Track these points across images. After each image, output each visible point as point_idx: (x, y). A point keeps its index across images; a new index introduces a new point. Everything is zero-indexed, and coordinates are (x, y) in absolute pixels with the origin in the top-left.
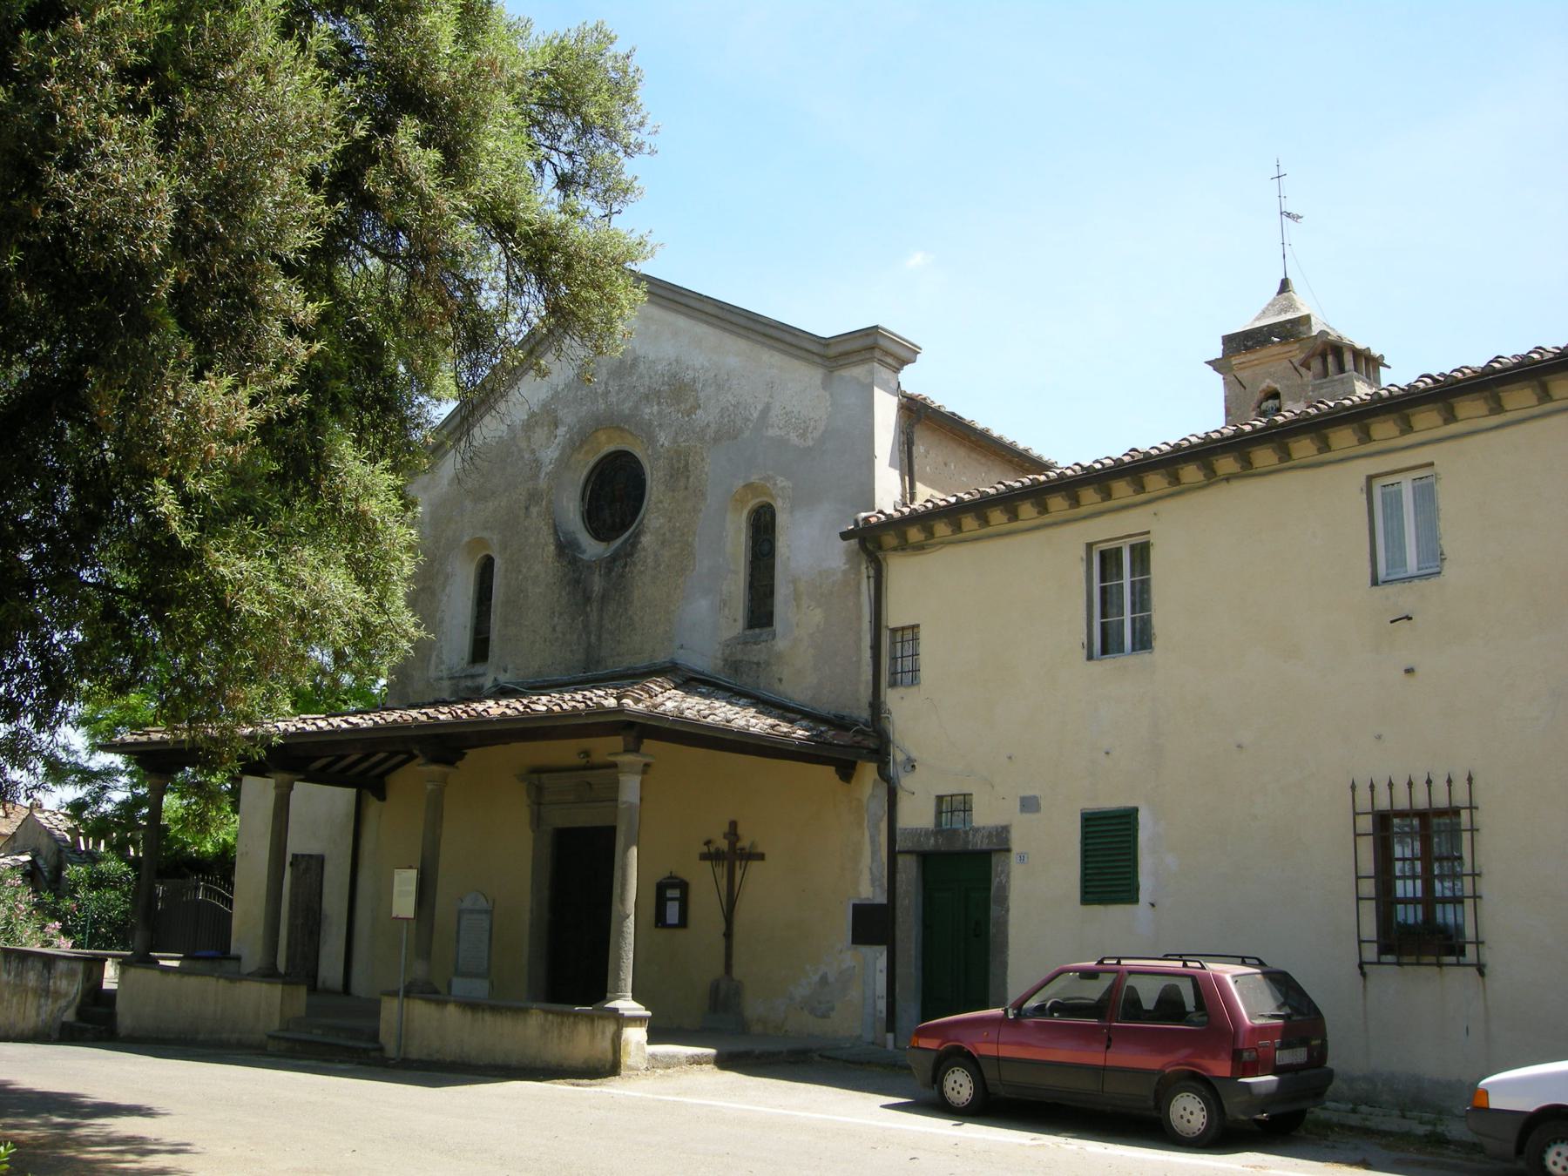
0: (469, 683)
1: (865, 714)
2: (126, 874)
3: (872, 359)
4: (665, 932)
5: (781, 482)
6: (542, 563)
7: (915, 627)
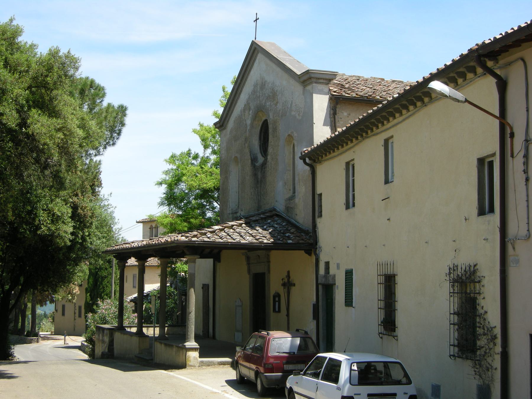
1: (310, 227)
2: (173, 292)
3: (311, 83)
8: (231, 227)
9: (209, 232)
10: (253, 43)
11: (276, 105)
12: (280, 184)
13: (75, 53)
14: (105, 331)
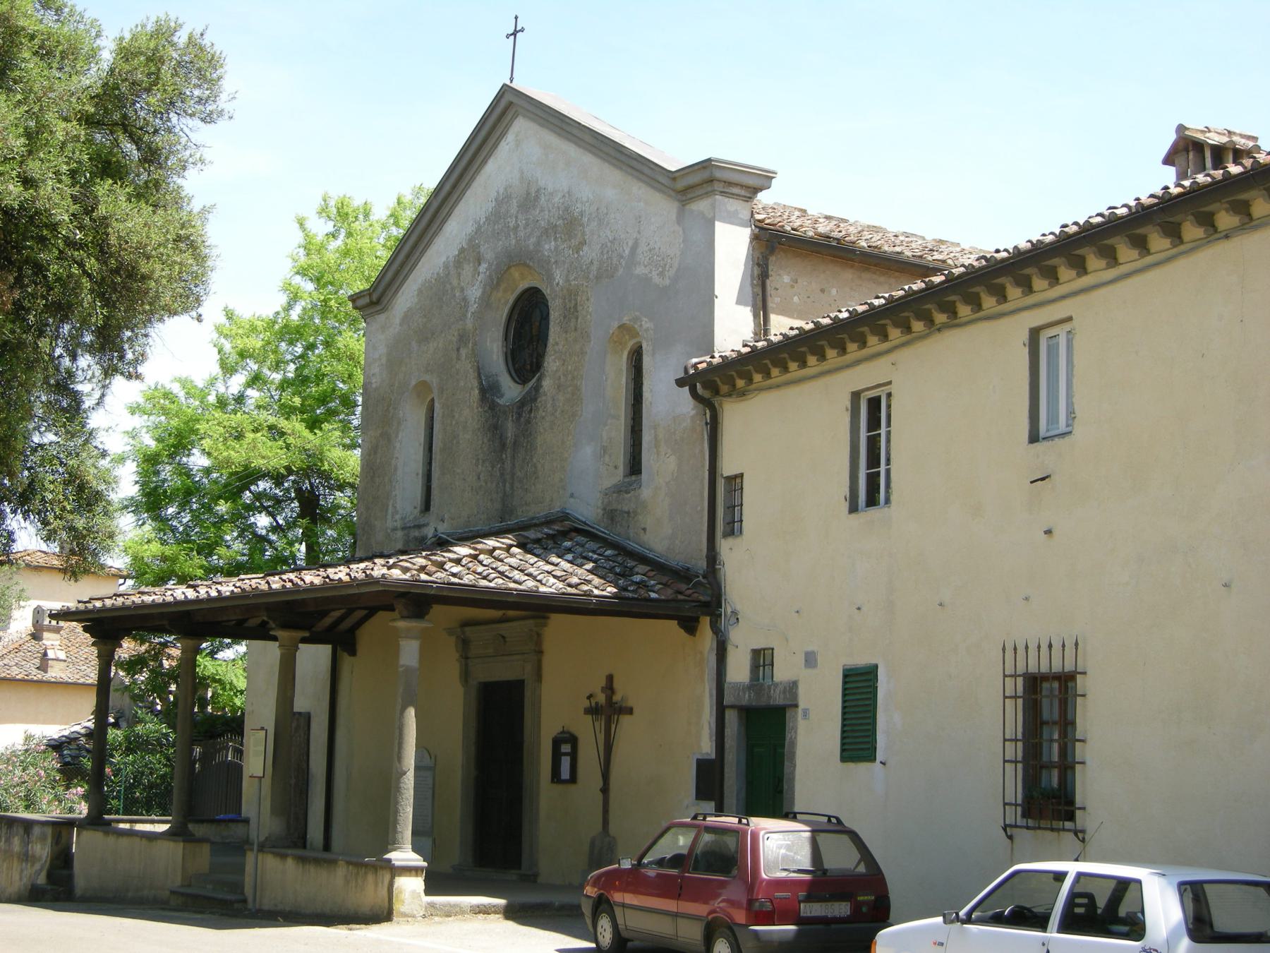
0: (416, 533)
1: (702, 564)
2: (166, 735)
3: (713, 192)
4: (560, 787)
5: (646, 324)
6: (469, 413)
7: (742, 475)
8: (491, 552)
9: (451, 560)
10: (505, 90)
11: (578, 249)
12: (587, 452)
13: (216, 41)
14: (37, 830)
